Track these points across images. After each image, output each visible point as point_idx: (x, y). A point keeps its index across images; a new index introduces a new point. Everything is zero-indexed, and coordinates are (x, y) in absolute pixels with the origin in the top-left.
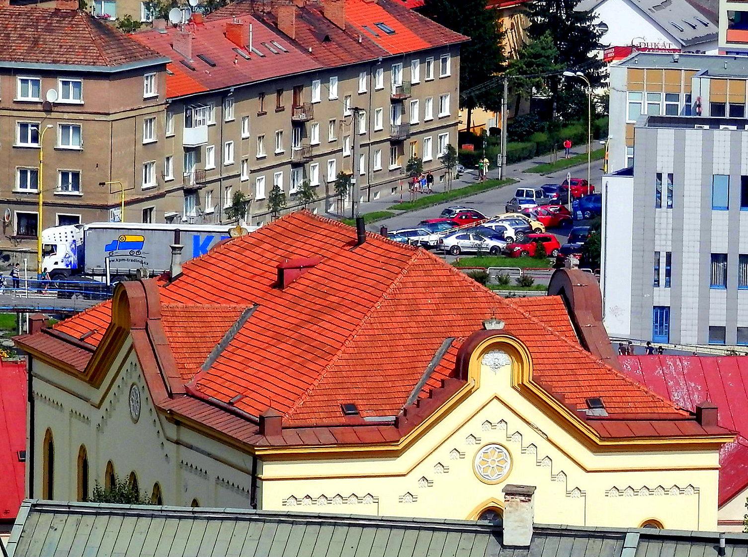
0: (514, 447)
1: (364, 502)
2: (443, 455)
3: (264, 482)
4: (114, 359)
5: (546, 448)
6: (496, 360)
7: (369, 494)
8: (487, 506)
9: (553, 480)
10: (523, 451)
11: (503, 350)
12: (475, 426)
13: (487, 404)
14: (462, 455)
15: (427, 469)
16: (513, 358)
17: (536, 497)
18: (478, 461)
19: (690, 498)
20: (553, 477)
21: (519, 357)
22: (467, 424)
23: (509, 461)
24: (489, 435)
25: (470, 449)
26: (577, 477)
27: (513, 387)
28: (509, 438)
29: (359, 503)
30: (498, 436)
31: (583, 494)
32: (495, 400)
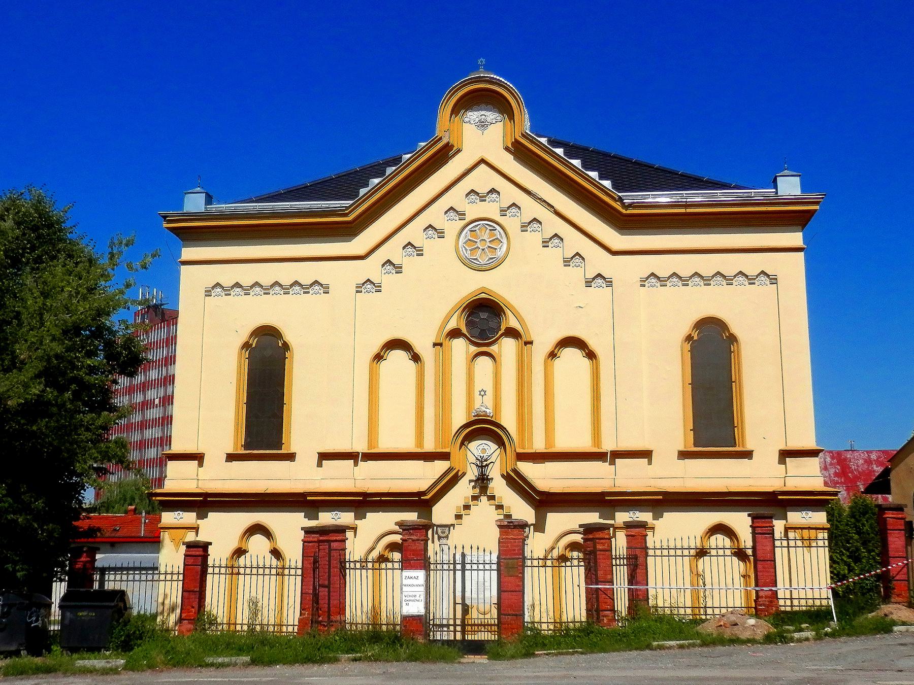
0: (512, 223)
1: (252, 294)
2: (413, 232)
3: (183, 268)
7: (653, 274)
8: (504, 307)
11: (492, 105)
12: (455, 197)
14: (441, 234)
15: (392, 250)
17: (203, 293)
18: (462, 240)
19: (764, 289)
23: (505, 240)
24: (474, 210)
25: (452, 227)
26: (598, 261)
27: (507, 149)
28: (503, 212)
29: (683, 285)
30: (490, 209)
31: (609, 283)
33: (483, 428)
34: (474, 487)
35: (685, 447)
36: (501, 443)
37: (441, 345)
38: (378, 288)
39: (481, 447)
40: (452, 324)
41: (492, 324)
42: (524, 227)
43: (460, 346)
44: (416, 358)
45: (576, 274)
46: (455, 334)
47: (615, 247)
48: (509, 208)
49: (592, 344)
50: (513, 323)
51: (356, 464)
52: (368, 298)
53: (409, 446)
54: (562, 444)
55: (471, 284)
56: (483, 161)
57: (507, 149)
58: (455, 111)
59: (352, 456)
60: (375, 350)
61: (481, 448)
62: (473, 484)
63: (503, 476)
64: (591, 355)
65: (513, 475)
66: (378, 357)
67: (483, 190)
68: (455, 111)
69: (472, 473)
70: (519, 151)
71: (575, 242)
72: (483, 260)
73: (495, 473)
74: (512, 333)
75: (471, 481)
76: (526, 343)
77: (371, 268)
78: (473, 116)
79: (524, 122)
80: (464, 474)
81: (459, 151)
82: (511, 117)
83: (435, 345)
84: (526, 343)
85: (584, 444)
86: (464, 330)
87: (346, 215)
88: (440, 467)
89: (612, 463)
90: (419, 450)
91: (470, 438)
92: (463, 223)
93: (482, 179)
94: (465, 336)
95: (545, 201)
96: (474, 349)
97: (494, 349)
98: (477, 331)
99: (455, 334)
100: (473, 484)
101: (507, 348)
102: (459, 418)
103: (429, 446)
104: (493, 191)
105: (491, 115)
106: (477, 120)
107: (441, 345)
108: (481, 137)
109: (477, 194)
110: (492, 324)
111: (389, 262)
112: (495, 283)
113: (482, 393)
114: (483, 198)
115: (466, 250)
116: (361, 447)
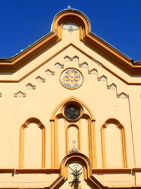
0: (84, 70)
2: (41, 72)
4: (108, 50)
5: (102, 72)
6: (71, 27)
7: (20, 92)
9: (90, 74)
10: (90, 72)
11: (75, 23)
12: (60, 58)
13: (102, 150)
14: (53, 73)
15: (31, 79)
16: (81, 27)
20: (109, 87)
21: (83, 25)
22: (19, 146)
23: (81, 77)
24: (68, 64)
25: (58, 70)
26: (122, 87)
28: (80, 65)
30: (75, 64)
31: (128, 97)
32: (113, 85)
33: (75, 157)
34: (71, 186)
35: (103, 168)
36: (84, 164)
37: (54, 121)
38: (24, 95)
39: (75, 166)
40: (59, 112)
41: (77, 113)
42: (90, 72)
43: (62, 123)
44: (42, 127)
45: (112, 91)
46: (60, 116)
47: (129, 82)
48: (83, 64)
49: (121, 122)
50: (86, 112)
51: (13, 175)
52: (20, 97)
53: (38, 166)
54: (109, 166)
55: (67, 95)
56: (71, 44)
57: (81, 40)
58: (59, 23)
59: (11, 171)
60: (23, 122)
61: (76, 167)
62: (71, 184)
63: (85, 180)
64: (121, 127)
65: (91, 179)
66: (24, 126)
67: (71, 56)
68: (59, 23)
69: (71, 178)
70: (87, 41)
71: (112, 79)
72: (72, 85)
73: (81, 178)
74: (86, 117)
75: (70, 183)
76: (92, 121)
77: (21, 86)
78: (67, 27)
79: (88, 28)
80: (67, 179)
81: (61, 40)
82: (84, 27)
83: (51, 121)
84: (92, 121)
85: (120, 166)
86: (64, 115)
87: (11, 62)
88: (55, 177)
89: (134, 174)
90: (125, 168)
91: (69, 162)
92: (63, 69)
93: (71, 52)
94: (64, 117)
95: (98, 62)
96: (69, 124)
97: (77, 123)
98: (69, 116)
99: (60, 116)
100: (71, 184)
101: (83, 123)
102: (62, 154)
103: (48, 166)
104: (76, 57)
105: (74, 27)
106: (68, 28)
107: (54, 121)
108: (70, 35)
109: (69, 58)
110: (77, 113)
111: (30, 84)
112: (78, 95)
113: (74, 142)
114: (71, 60)
115: (64, 81)
116: (16, 167)
